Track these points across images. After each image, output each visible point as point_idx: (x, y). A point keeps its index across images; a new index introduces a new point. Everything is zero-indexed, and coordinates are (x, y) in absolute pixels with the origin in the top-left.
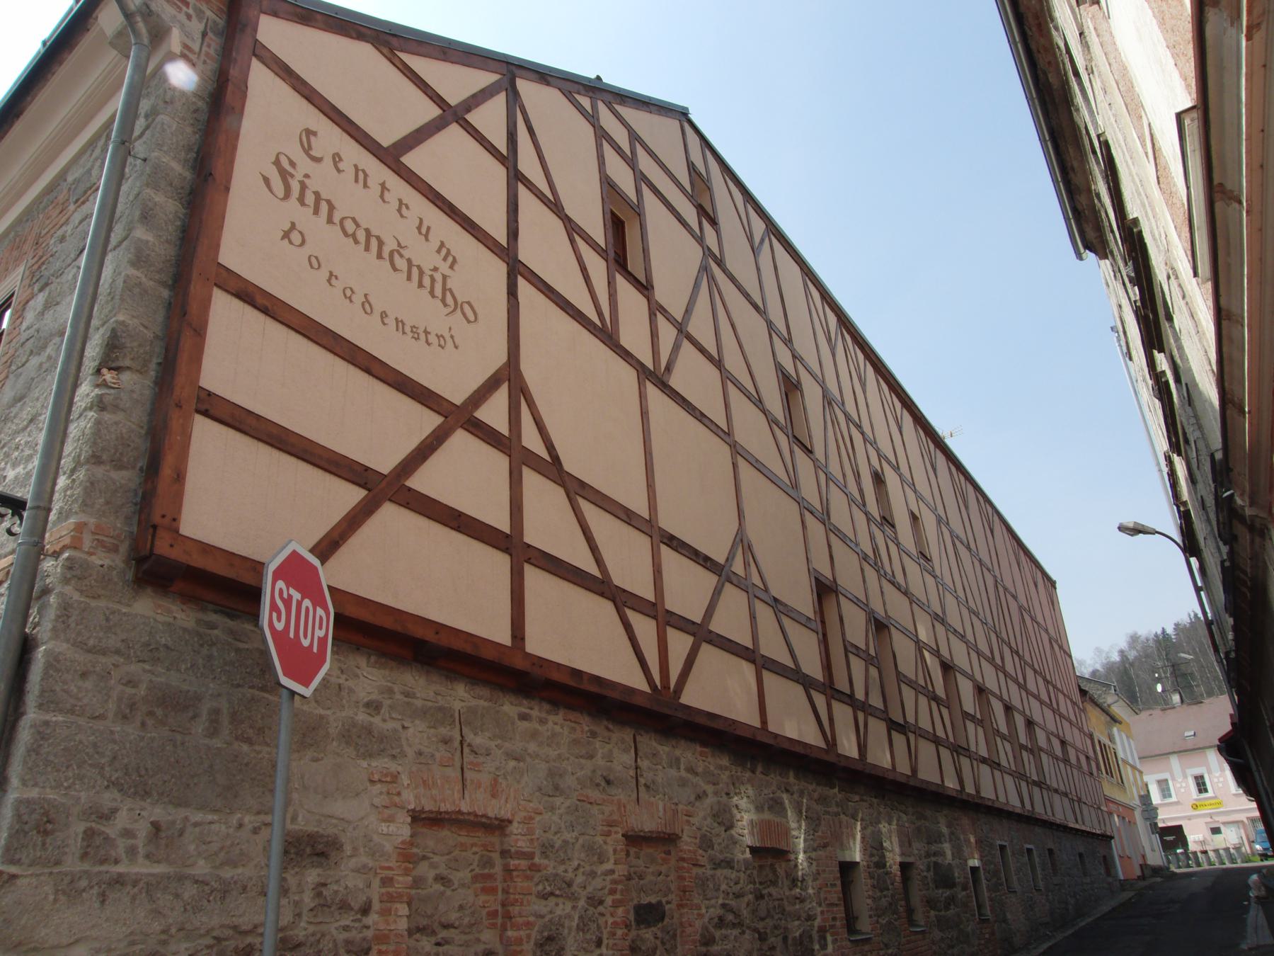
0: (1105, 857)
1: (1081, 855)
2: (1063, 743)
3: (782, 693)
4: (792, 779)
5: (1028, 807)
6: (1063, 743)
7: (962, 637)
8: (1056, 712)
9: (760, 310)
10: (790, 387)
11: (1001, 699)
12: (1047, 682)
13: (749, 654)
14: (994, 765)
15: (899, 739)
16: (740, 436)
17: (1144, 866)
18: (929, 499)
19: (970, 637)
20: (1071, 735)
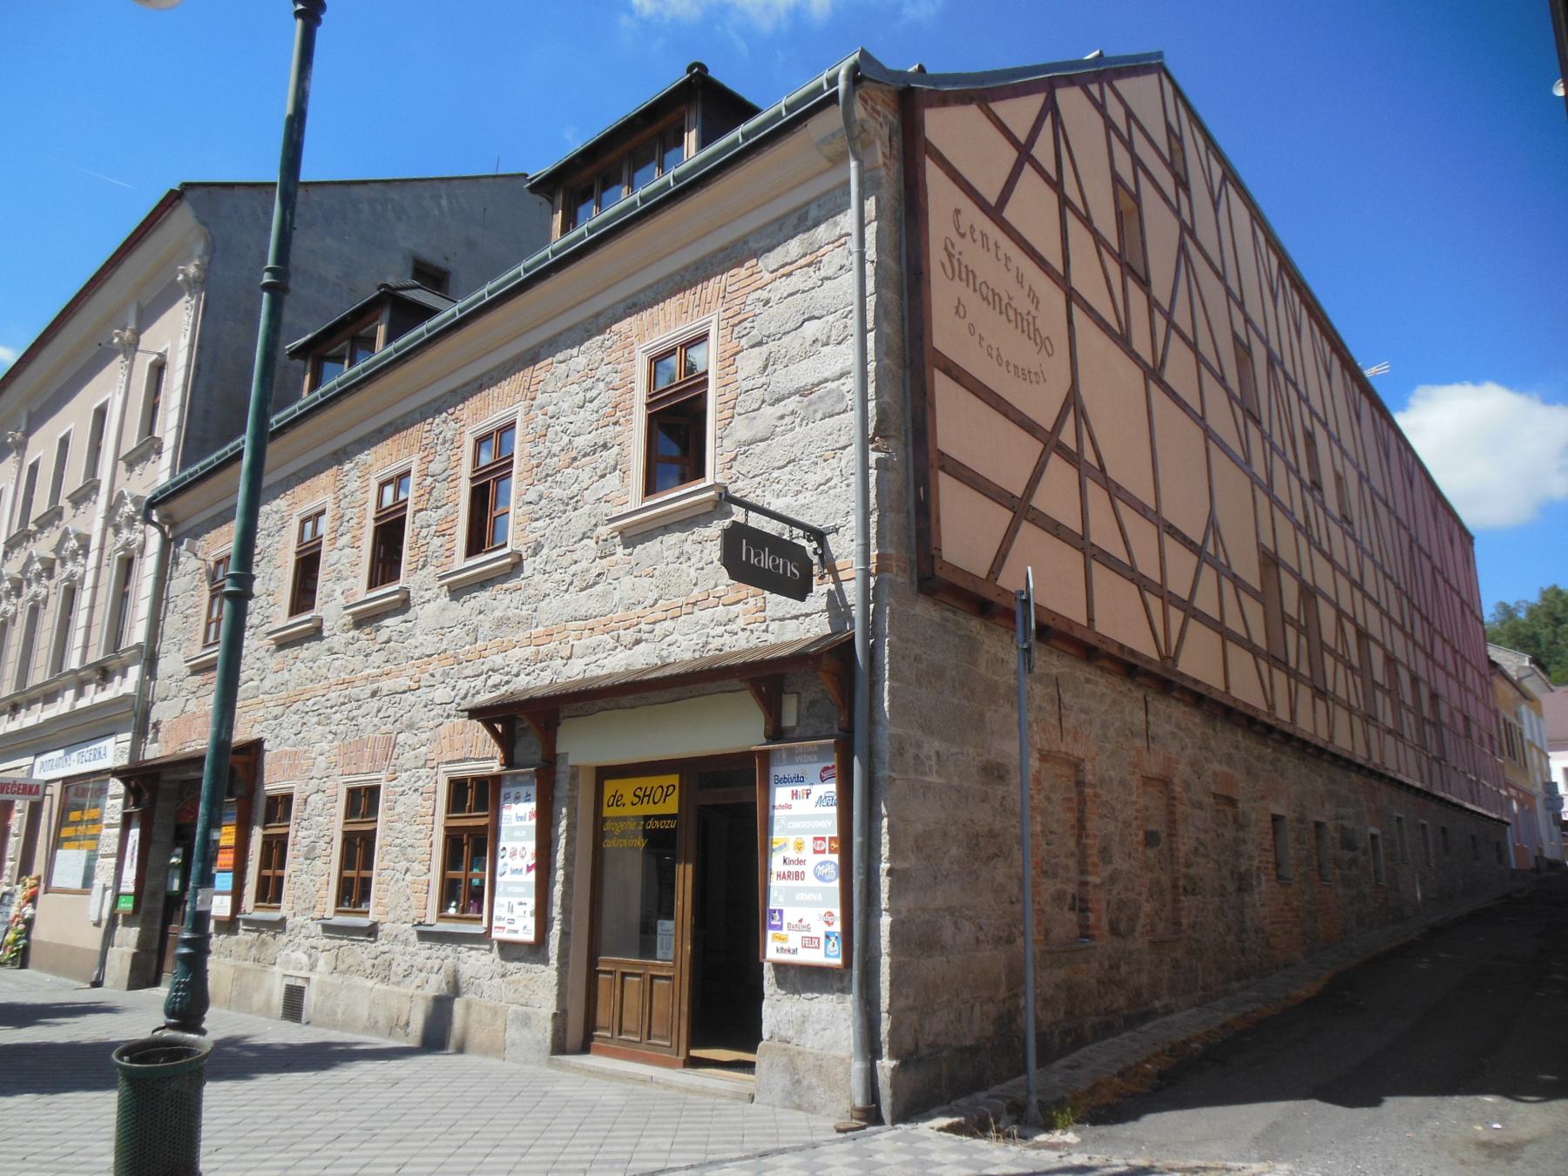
0: (1498, 844)
1: (1473, 838)
2: (1466, 719)
3: (1241, 661)
4: (1240, 738)
5: (1376, 760)
6: (1466, 719)
7: (1377, 604)
8: (1462, 684)
9: (1221, 277)
10: (1243, 351)
11: (1297, 576)
12: (1455, 652)
13: (1080, 542)
14: (1397, 734)
15: (1320, 705)
16: (1076, 283)
17: (1539, 858)
18: (1353, 455)
19: (1383, 604)
20: (1477, 712)
